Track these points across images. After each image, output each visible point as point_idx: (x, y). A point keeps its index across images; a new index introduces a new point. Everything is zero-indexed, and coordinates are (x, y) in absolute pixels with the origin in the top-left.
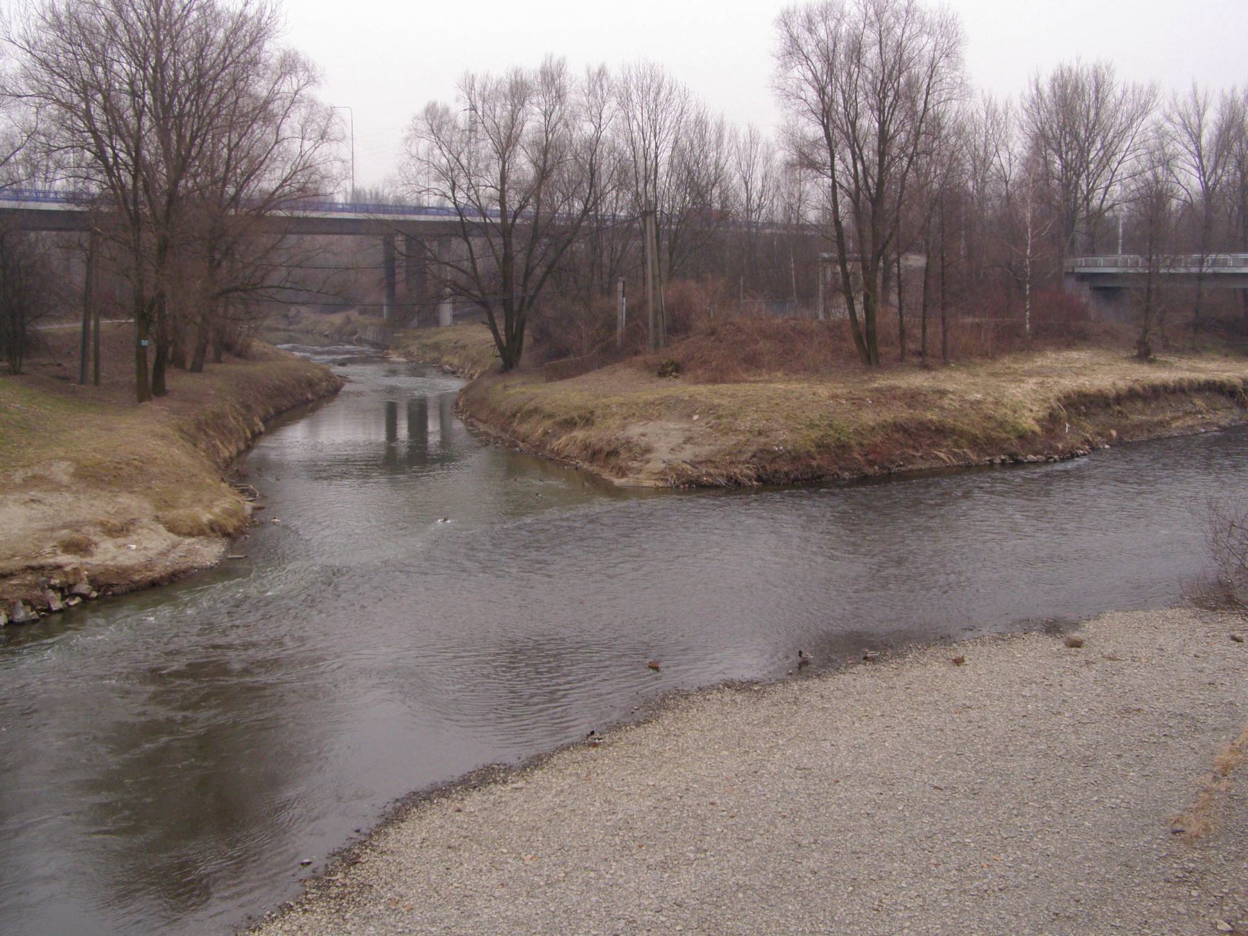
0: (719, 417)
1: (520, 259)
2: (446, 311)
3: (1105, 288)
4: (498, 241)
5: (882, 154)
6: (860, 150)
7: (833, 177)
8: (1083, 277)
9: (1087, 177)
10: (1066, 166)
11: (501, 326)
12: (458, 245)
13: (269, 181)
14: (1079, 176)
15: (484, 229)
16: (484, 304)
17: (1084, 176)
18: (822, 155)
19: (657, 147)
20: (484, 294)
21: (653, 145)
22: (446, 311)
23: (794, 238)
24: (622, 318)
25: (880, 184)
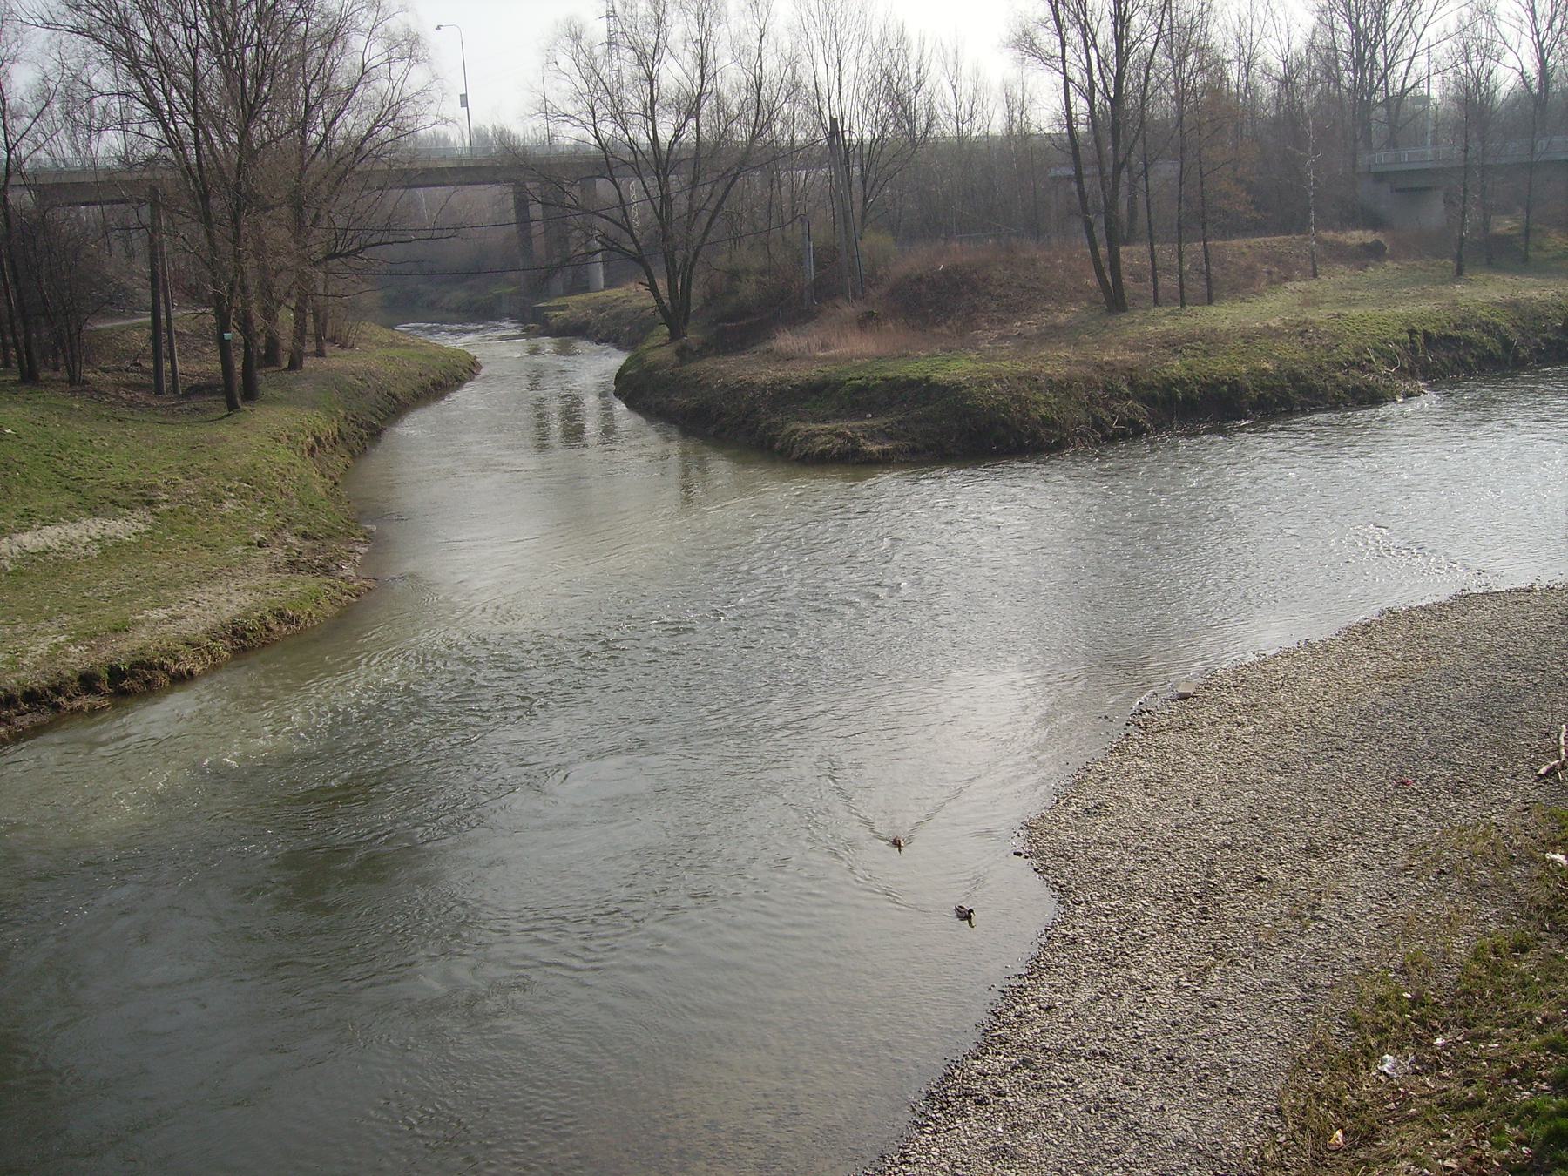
0: (1106, 497)
1: (681, 204)
2: (599, 273)
3: (1411, 190)
4: (651, 181)
5: (1119, 39)
6: (1094, 36)
7: (1065, 73)
8: (1380, 177)
9: (1385, 48)
10: (1358, 35)
11: (662, 285)
12: (603, 187)
13: (352, 124)
14: (1375, 47)
15: (636, 169)
16: (639, 260)
17: (1380, 48)
18: (1048, 41)
19: (839, 50)
20: (639, 248)
21: (834, 47)
22: (599, 273)
23: (1020, 147)
24: (339, 867)
25: (1119, 77)
